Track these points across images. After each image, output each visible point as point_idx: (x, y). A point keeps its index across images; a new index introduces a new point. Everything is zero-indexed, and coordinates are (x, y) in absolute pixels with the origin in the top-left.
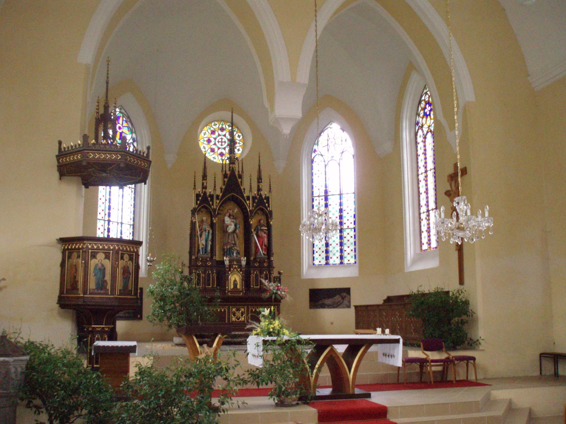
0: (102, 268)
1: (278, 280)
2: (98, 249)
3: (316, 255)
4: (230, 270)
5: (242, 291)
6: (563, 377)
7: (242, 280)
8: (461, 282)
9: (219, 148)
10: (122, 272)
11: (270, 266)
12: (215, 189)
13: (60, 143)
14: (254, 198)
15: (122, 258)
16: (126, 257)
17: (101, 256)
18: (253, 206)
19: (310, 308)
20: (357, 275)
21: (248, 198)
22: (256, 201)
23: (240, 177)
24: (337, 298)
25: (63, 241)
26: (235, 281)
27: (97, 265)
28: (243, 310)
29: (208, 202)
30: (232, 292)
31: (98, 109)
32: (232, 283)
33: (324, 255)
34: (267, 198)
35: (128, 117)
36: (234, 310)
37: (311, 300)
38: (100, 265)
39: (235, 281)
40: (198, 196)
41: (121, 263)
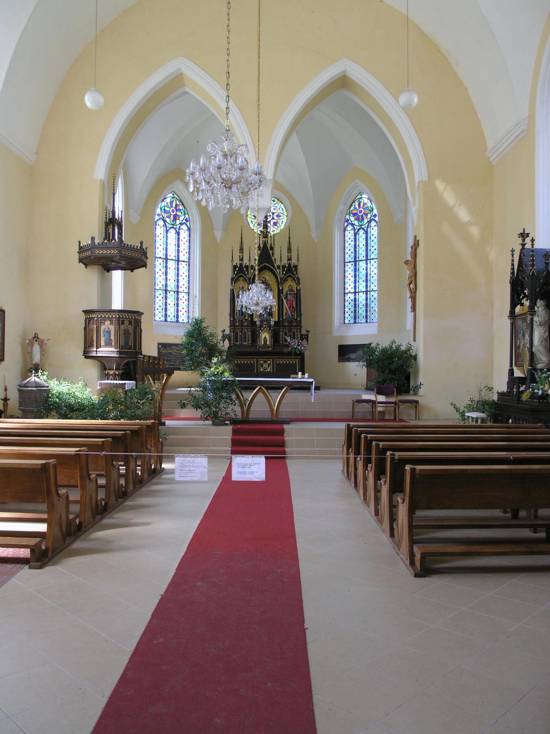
1: (305, 337)
2: (126, 318)
3: (347, 315)
4: (261, 329)
5: (270, 347)
9: (273, 218)
12: (250, 261)
13: (80, 242)
14: (284, 267)
15: (123, 323)
16: (126, 322)
17: (108, 323)
18: (283, 274)
19: (339, 362)
21: (279, 267)
22: (286, 269)
23: (272, 248)
25: (86, 312)
26: (265, 338)
27: (105, 328)
28: (269, 362)
29: (244, 273)
31: (106, 215)
32: (263, 340)
33: (352, 315)
34: (296, 267)
35: (182, 203)
36: (262, 362)
39: (265, 338)
40: (235, 267)
41: (122, 327)
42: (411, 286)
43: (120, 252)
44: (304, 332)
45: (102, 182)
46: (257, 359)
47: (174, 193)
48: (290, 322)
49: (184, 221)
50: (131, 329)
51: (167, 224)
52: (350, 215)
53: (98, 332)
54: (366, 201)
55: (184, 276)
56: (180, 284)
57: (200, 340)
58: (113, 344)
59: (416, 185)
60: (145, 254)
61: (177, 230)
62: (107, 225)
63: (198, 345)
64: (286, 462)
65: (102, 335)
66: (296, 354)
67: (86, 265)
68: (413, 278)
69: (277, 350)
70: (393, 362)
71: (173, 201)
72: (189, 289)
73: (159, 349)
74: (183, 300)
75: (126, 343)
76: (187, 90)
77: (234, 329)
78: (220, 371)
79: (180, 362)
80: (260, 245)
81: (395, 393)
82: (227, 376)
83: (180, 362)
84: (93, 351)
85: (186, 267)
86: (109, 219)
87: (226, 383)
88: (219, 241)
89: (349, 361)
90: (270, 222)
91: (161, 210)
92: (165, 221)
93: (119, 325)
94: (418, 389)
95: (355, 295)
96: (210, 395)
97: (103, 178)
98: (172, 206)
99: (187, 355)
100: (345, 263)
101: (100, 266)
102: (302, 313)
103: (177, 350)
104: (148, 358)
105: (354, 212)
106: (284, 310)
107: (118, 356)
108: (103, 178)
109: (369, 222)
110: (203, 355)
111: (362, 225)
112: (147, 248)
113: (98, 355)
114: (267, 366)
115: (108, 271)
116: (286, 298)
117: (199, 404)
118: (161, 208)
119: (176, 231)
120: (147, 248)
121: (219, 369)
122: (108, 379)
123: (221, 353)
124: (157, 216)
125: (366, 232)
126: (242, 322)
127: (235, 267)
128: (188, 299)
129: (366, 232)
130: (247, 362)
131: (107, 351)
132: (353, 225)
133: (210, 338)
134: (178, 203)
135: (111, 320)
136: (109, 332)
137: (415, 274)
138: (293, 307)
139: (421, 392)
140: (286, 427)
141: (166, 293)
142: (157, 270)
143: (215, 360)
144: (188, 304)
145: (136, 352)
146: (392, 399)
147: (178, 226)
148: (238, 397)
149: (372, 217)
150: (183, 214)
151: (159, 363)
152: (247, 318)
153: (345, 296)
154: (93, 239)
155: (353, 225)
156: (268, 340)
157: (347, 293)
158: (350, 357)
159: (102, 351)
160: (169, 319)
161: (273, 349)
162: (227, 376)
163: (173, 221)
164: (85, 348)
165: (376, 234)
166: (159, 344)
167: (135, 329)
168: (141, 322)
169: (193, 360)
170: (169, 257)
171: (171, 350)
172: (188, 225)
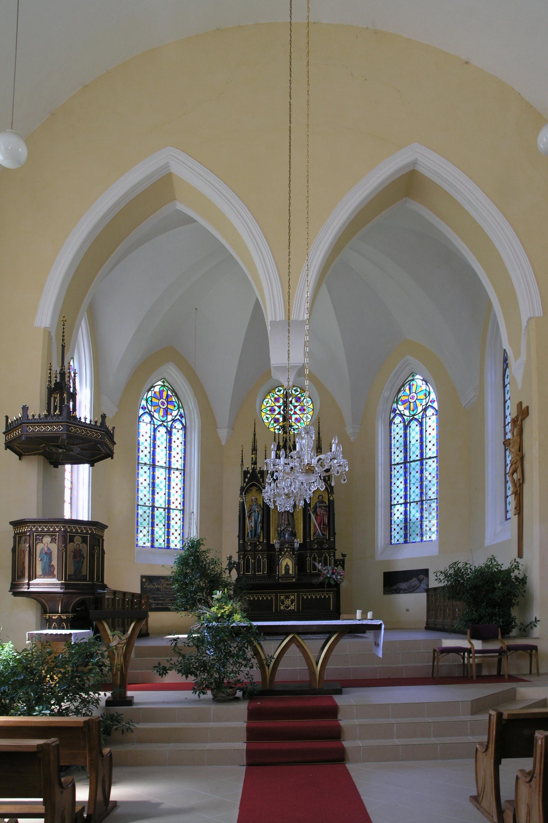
0: (49, 552)
1: (341, 563)
2: (76, 532)
4: (281, 554)
5: (294, 577)
6: (545, 674)
7: (295, 565)
8: (520, 555)
10: (72, 556)
11: (332, 548)
13: (7, 418)
15: (72, 540)
19: (384, 594)
20: (437, 554)
24: (414, 581)
25: (16, 524)
26: (287, 565)
27: (43, 549)
28: (292, 597)
30: (283, 577)
31: (50, 377)
32: (283, 568)
35: (176, 394)
36: (282, 597)
37: (385, 585)
38: (46, 549)
39: (287, 565)
40: (246, 473)
41: (71, 546)
42: (515, 476)
43: (68, 428)
44: (338, 556)
45: (47, 332)
46: (276, 594)
47: (164, 380)
48: (320, 543)
49: (178, 417)
50: (85, 549)
51: (155, 420)
52: (397, 403)
53: (32, 554)
54: (420, 382)
55: (177, 488)
56: (172, 499)
57: (198, 568)
58: (55, 573)
59: (524, 324)
60: (110, 435)
61: (169, 429)
62: (51, 392)
63: (194, 575)
64: (347, 770)
65: (38, 559)
66: (329, 585)
67: (20, 456)
68: (519, 464)
69: (304, 579)
70: (495, 589)
71: (163, 390)
72: (183, 505)
73: (142, 584)
74: (176, 519)
75: (78, 571)
76: (180, 206)
77: (244, 556)
78: (227, 613)
79: (171, 600)
80: (279, 443)
81: (500, 637)
82: (238, 620)
83: (171, 600)
84: (24, 584)
85: (180, 477)
86: (56, 384)
87: (237, 632)
88: (223, 443)
89: (399, 593)
90: (291, 418)
91: (147, 402)
92: (152, 416)
93: (65, 542)
94: (532, 628)
95: (406, 507)
96: (210, 652)
97: (48, 325)
98: (161, 397)
99: (178, 591)
100: (391, 465)
101: (42, 457)
102: (336, 532)
103: (167, 584)
104: (130, 596)
105: (403, 398)
106: (312, 528)
107: (62, 591)
108: (48, 325)
109: (425, 410)
110: (202, 589)
111: (415, 415)
112: (114, 428)
113: (31, 590)
114: (290, 603)
115: (56, 466)
116: (315, 512)
117: (190, 668)
118: (147, 400)
119: (167, 429)
120: (114, 428)
121: (225, 609)
122: (50, 628)
123: (226, 585)
124: (141, 410)
125: (421, 424)
126: (254, 545)
127: (246, 473)
128: (183, 518)
129: (421, 424)
130: (263, 598)
131: (44, 583)
132: (401, 415)
133: (212, 567)
134: (169, 393)
135: (52, 535)
136: (49, 554)
137: (520, 459)
138: (324, 524)
139: (536, 632)
140: (339, 700)
141: (153, 511)
142: (141, 480)
143: (218, 594)
144: (183, 525)
145: (94, 585)
146: (495, 645)
147: (170, 423)
148: (256, 653)
149: (429, 404)
150: (176, 408)
151: (140, 602)
152: (261, 540)
153: (391, 509)
154: (25, 409)
155: (401, 415)
156: (291, 568)
157: (395, 505)
158: (400, 587)
159: (38, 584)
160: (156, 544)
161: (298, 580)
162: (238, 620)
163: (163, 417)
164: (13, 579)
165: (434, 425)
166: (142, 577)
167: (92, 549)
168: (103, 540)
169: (186, 597)
170: (157, 464)
171: (158, 584)
172: (184, 421)
